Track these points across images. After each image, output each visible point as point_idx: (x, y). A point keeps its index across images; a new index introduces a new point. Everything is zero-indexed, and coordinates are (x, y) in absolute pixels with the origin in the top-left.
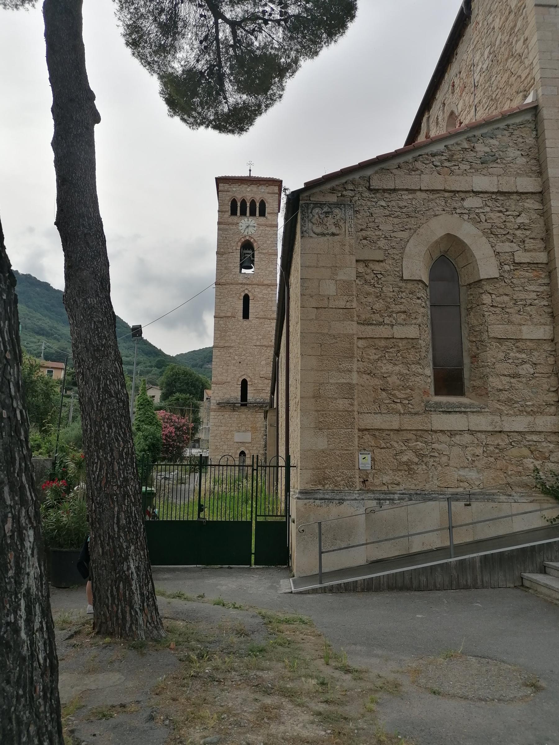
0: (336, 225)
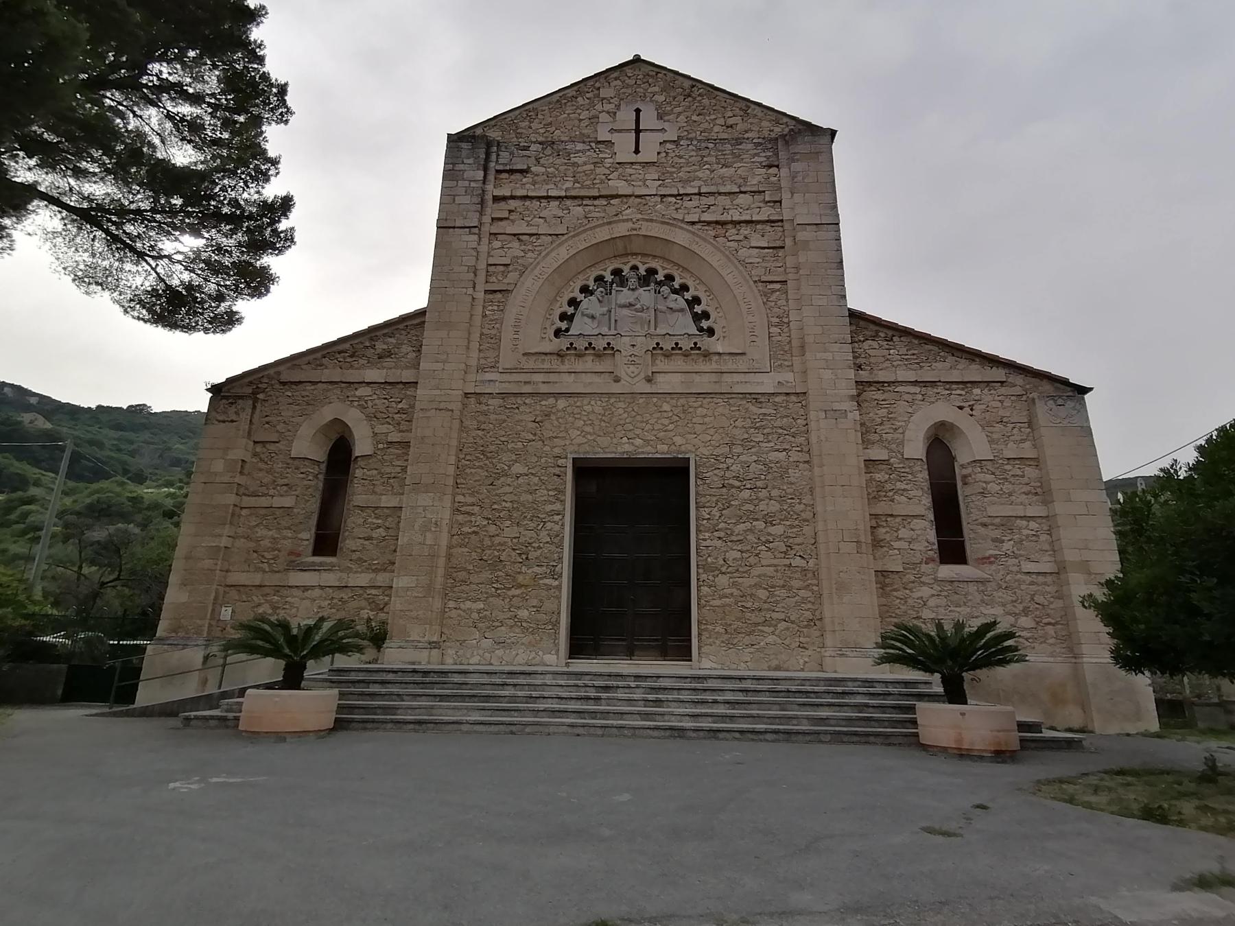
0: (237, 413)
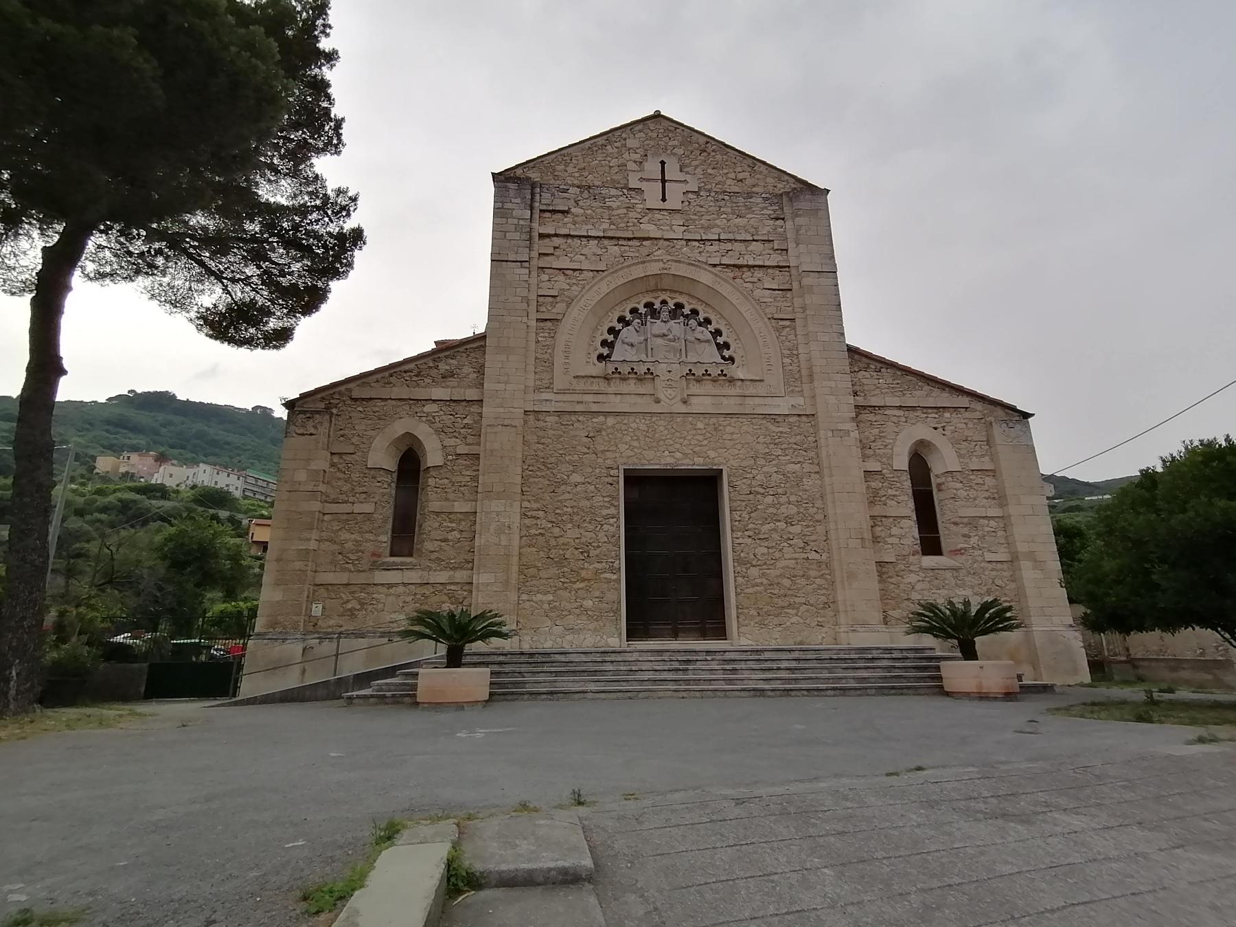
0: (315, 427)
